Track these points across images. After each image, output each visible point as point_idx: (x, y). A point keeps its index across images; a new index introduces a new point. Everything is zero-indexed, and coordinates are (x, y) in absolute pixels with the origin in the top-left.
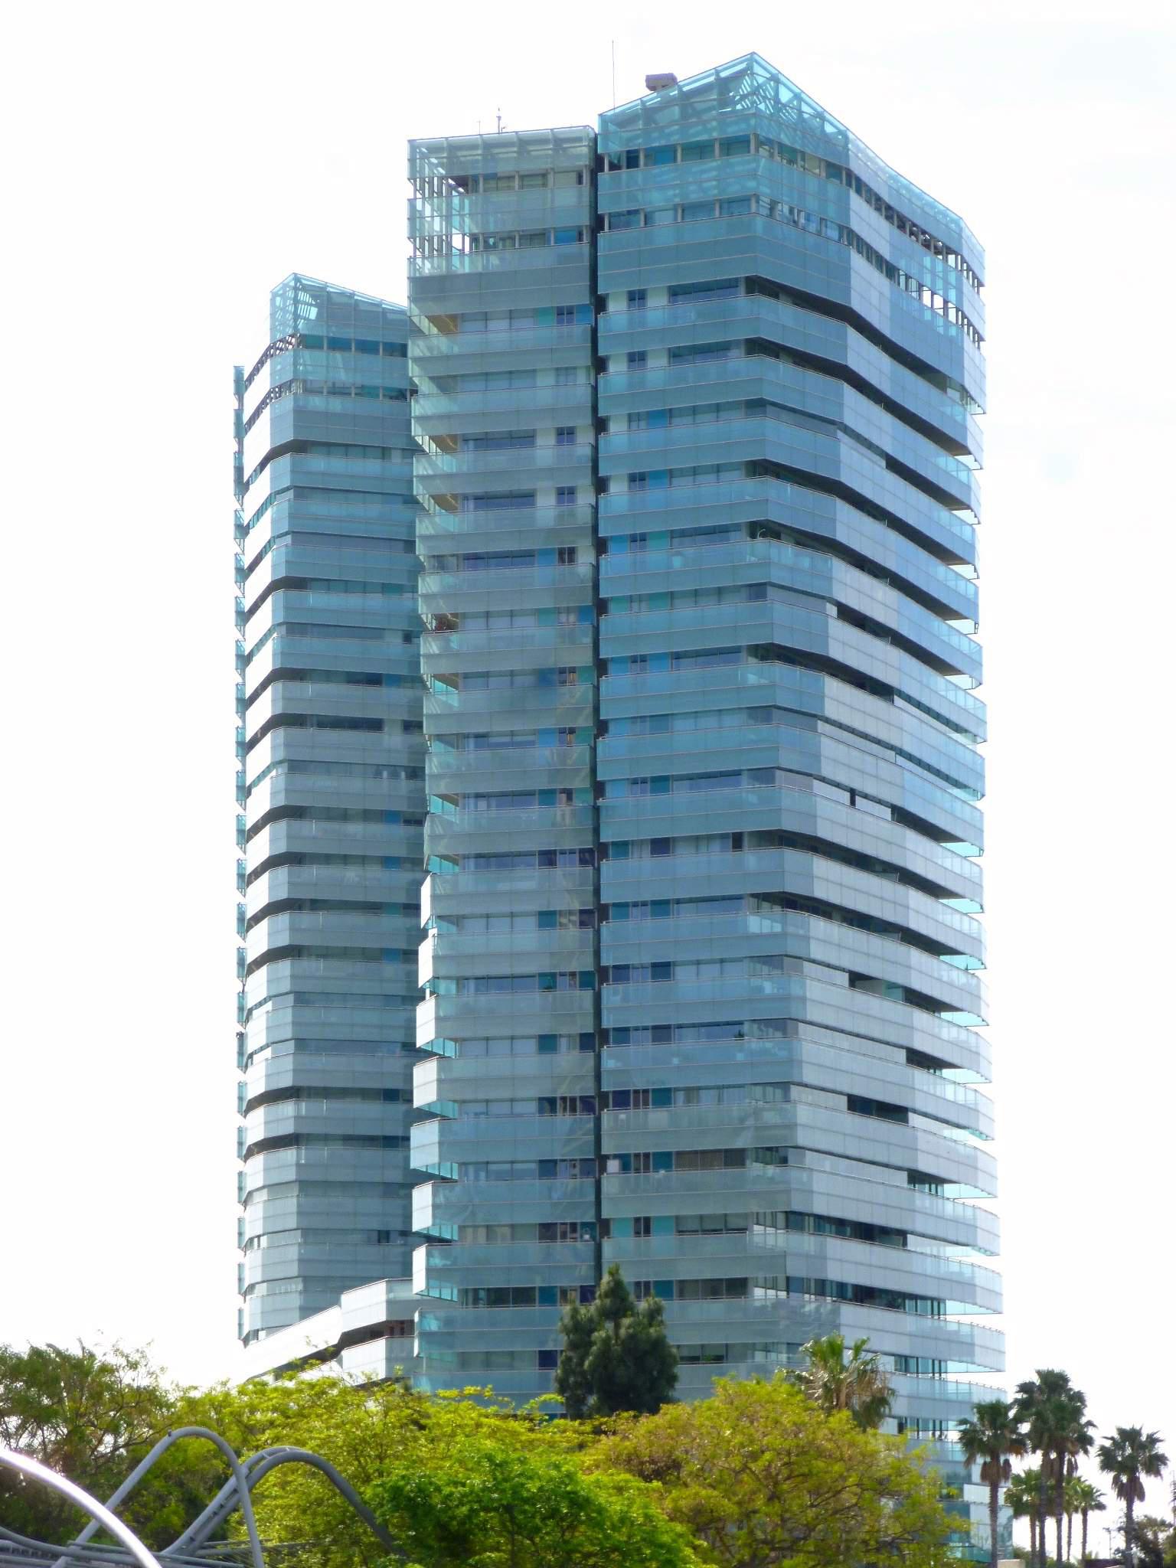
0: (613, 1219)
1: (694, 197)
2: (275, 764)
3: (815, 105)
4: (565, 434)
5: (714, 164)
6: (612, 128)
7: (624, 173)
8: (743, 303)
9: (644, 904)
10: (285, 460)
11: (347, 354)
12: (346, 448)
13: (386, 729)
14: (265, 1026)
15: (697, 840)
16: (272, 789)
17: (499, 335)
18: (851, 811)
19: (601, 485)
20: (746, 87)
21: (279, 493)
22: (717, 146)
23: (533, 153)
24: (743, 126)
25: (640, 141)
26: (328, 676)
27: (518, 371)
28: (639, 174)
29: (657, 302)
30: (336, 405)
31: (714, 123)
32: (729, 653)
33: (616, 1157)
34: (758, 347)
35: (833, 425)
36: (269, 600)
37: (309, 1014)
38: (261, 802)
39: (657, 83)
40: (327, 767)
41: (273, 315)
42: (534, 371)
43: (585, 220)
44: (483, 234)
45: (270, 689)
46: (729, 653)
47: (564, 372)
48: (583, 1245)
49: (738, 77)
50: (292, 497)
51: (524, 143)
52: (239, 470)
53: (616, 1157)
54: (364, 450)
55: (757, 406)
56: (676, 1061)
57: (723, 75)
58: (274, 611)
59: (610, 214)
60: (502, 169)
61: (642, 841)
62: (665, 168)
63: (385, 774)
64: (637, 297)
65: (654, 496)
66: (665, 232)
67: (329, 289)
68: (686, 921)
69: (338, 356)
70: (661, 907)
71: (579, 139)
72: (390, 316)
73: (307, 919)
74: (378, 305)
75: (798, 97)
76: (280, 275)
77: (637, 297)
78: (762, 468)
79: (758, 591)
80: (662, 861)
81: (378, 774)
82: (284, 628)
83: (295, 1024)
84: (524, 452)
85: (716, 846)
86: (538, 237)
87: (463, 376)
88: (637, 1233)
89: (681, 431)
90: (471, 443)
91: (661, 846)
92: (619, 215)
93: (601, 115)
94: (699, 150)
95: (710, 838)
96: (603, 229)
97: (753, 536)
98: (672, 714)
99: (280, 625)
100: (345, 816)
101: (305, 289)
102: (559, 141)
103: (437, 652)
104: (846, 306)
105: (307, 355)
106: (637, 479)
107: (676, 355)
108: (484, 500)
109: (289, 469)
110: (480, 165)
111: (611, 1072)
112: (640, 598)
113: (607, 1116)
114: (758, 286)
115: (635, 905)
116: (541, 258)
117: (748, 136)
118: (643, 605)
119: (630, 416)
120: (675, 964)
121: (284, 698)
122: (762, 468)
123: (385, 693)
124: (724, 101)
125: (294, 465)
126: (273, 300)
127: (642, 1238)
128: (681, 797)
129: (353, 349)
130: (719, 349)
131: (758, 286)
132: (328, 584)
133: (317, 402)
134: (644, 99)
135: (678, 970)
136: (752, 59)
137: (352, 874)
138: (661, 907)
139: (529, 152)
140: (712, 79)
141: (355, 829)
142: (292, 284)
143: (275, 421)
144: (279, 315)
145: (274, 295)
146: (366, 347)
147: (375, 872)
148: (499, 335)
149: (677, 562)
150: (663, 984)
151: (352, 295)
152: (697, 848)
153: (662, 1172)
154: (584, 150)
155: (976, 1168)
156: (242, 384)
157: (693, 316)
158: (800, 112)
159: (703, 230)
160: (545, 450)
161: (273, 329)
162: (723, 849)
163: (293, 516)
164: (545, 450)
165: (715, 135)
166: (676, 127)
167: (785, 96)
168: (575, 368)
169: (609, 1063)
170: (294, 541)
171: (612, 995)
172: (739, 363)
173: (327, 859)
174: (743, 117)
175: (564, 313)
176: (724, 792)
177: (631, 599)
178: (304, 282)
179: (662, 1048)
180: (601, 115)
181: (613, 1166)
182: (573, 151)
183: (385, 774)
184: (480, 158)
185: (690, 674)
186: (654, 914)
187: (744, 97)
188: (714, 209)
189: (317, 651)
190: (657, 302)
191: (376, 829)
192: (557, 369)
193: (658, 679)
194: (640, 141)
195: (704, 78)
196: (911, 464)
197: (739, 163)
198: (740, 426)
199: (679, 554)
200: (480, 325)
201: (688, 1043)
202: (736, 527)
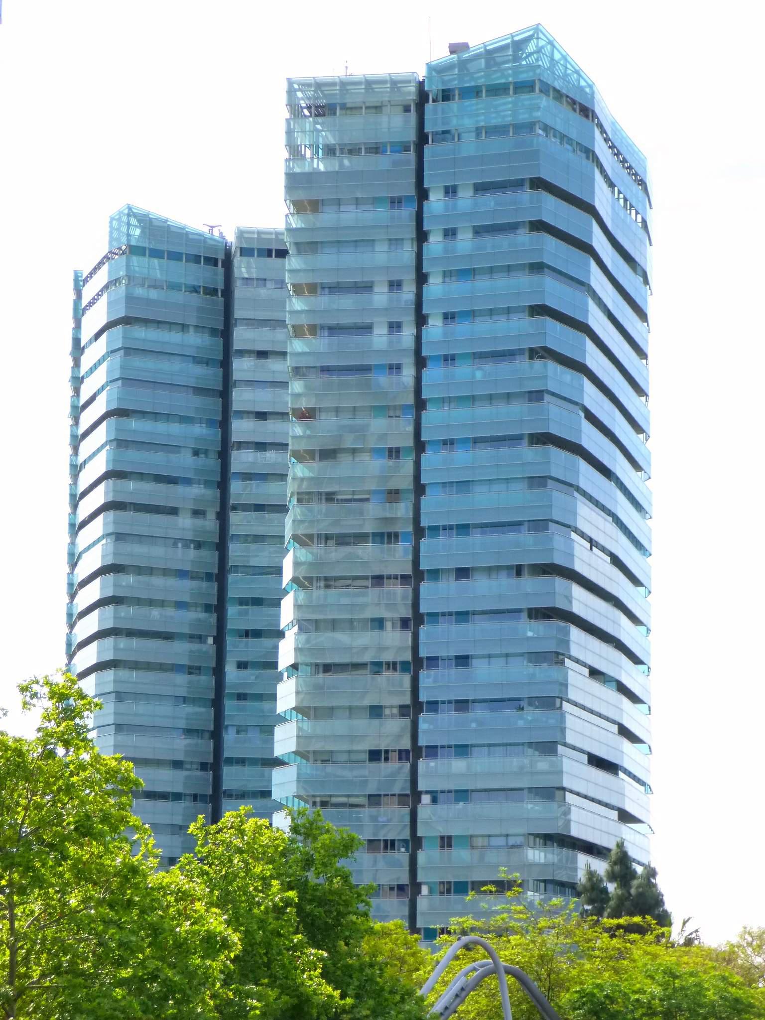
0: (425, 837)
1: (495, 122)
2: (106, 535)
3: (575, 65)
4: (395, 285)
5: (510, 99)
6: (434, 73)
7: (441, 104)
8: (526, 195)
9: (450, 614)
10: (119, 330)
11: (162, 261)
12: (158, 323)
13: (180, 515)
14: (294, 690)
15: (490, 570)
16: (102, 552)
17: (348, 215)
18: (589, 553)
19: (421, 320)
20: (531, 47)
21: (113, 352)
22: (511, 87)
23: (376, 90)
24: (531, 74)
25: (456, 82)
26: (141, 476)
27: (363, 241)
28: (454, 105)
29: (466, 196)
30: (154, 294)
31: (510, 72)
32: (516, 439)
33: (427, 792)
34: (539, 226)
35: (584, 285)
36: (104, 424)
37: (123, 707)
38: (91, 562)
39: (455, 49)
40: (140, 538)
41: (111, 233)
42: (373, 240)
43: (411, 136)
44: (339, 144)
45: (103, 484)
46: (516, 439)
47: (395, 242)
48: (402, 855)
49: (527, 40)
50: (123, 354)
51: (370, 84)
52: (76, 341)
53: (427, 792)
54: (170, 325)
55: (538, 268)
56: (474, 725)
57: (516, 38)
58: (107, 432)
59: (433, 132)
60: (349, 101)
61: (449, 570)
62: (474, 101)
63: (180, 545)
64: (451, 191)
65: (461, 328)
66: (469, 146)
67: (151, 216)
68: (478, 628)
69: (156, 261)
70: (463, 616)
71: (409, 82)
72: (191, 236)
73: (123, 642)
74: (183, 229)
75: (564, 58)
76: (117, 205)
77: (451, 191)
78: (540, 310)
79: (536, 396)
80: (463, 583)
81: (175, 545)
82: (115, 443)
83: (115, 714)
84: (366, 296)
85: (504, 573)
86: (376, 149)
87: (322, 242)
88: (442, 847)
89: (482, 284)
90: (327, 290)
91: (463, 573)
92: (437, 133)
93: (427, 64)
94: (497, 90)
95: (499, 568)
96: (428, 143)
97: (531, 358)
98: (473, 481)
99: (111, 441)
100: (150, 571)
101: (135, 215)
102: (395, 84)
103: (301, 434)
104: (591, 205)
105: (135, 259)
106: (449, 317)
107: (478, 231)
108: (334, 330)
109: (121, 336)
110: (338, 97)
111: (425, 731)
112: (450, 400)
113: (422, 764)
114: (539, 184)
115: (444, 614)
116: (383, 162)
117: (534, 81)
118: (453, 405)
119: (444, 272)
120: (472, 657)
121: (114, 491)
122: (540, 310)
123: (180, 490)
124: (516, 58)
125: (125, 333)
126: (111, 222)
127: (446, 851)
128: (476, 539)
129: (166, 258)
130: (512, 227)
131: (539, 184)
132: (142, 414)
133: (139, 292)
134: (486, 44)
135: (475, 662)
136: (537, 30)
137: (155, 613)
138: (463, 616)
139: (373, 89)
140: (509, 41)
141: (158, 581)
142: (126, 211)
143: (110, 304)
144: (115, 235)
145: (112, 219)
146: (175, 256)
147: (170, 612)
148: (348, 215)
149: (479, 375)
150: (462, 670)
151: (166, 221)
152: (489, 575)
153: (461, 804)
154: (412, 89)
155: (624, 795)
156: (79, 283)
157: (492, 203)
158: (566, 68)
159: (497, 145)
160: (380, 296)
161: (110, 242)
162: (509, 576)
163: (123, 368)
164: (380, 296)
165: (510, 79)
166: (483, 73)
167: (557, 56)
168: (402, 239)
169: (423, 726)
170: (123, 385)
171: (427, 678)
172: (524, 237)
173: (138, 602)
174: (532, 68)
175: (396, 202)
176: (508, 537)
177: (443, 400)
178: (134, 210)
179: (462, 715)
180: (427, 64)
181: (426, 799)
182: (404, 89)
183: (180, 545)
184: (338, 92)
185: (484, 453)
186: (457, 621)
187: (531, 54)
188: (509, 131)
189: (136, 458)
190: (466, 196)
191: (172, 582)
192: (390, 240)
193: (462, 457)
194: (456, 82)
195: (496, 43)
196: (620, 319)
197: (525, 98)
198: (524, 281)
199: (479, 369)
200: (335, 208)
201: (477, 713)
202: (521, 352)
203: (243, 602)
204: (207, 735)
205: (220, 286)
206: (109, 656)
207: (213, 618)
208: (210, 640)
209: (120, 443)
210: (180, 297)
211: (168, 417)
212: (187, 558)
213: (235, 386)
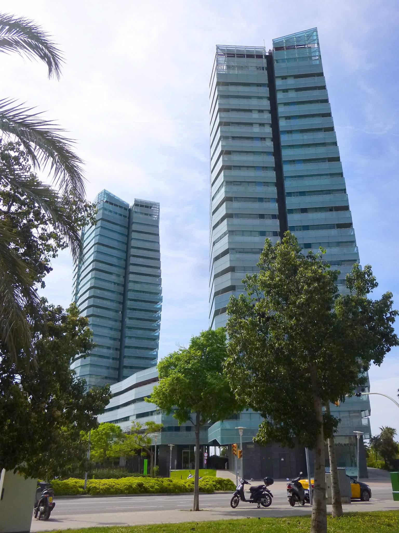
2: (95, 252)
30: (110, 214)
178: (106, 192)
203: (131, 309)
204: (118, 340)
205: (128, 216)
206: (91, 313)
207: (121, 306)
208: (120, 312)
209: (98, 252)
210: (118, 216)
211: (107, 299)
212: (109, 342)
213: (128, 291)
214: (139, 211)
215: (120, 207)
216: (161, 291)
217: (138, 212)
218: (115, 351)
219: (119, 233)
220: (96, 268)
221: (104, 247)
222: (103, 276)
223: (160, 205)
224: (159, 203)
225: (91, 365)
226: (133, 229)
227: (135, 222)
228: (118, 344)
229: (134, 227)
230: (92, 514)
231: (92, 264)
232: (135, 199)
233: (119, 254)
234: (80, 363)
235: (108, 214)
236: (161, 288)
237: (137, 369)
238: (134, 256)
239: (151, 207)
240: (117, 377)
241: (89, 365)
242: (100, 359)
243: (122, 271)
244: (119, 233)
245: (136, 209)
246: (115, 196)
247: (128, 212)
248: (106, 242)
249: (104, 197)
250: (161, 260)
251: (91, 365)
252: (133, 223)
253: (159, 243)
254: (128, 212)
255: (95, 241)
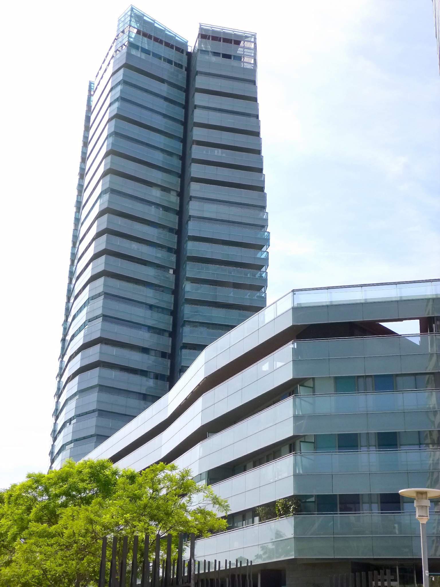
30: (143, 56)
204: (167, 334)
205: (185, 64)
208: (171, 271)
213: (183, 325)
214: (209, 49)
215: (167, 45)
216: (267, 240)
217: (208, 52)
218: (160, 359)
219: (166, 99)
220: (118, 113)
221: (125, 240)
222: (131, 188)
223: (257, 37)
224: (254, 36)
225: (102, 388)
226: (195, 120)
227: (194, 217)
228: (166, 342)
229: (200, 82)
230: (159, 54)
231: (94, 242)
232: (201, 25)
233: (159, 255)
234: (71, 435)
235: (139, 56)
236: (266, 233)
237: (222, 329)
238: (200, 143)
239: (238, 43)
240: (168, 373)
241: (95, 438)
242: (125, 376)
243: (174, 182)
244: (166, 99)
245: (202, 46)
246: (154, 21)
247: (186, 72)
248: (135, 113)
249: (130, 26)
250: (263, 153)
251: (102, 388)
252: (197, 73)
253: (257, 117)
254: (185, 57)
255: (95, 247)
